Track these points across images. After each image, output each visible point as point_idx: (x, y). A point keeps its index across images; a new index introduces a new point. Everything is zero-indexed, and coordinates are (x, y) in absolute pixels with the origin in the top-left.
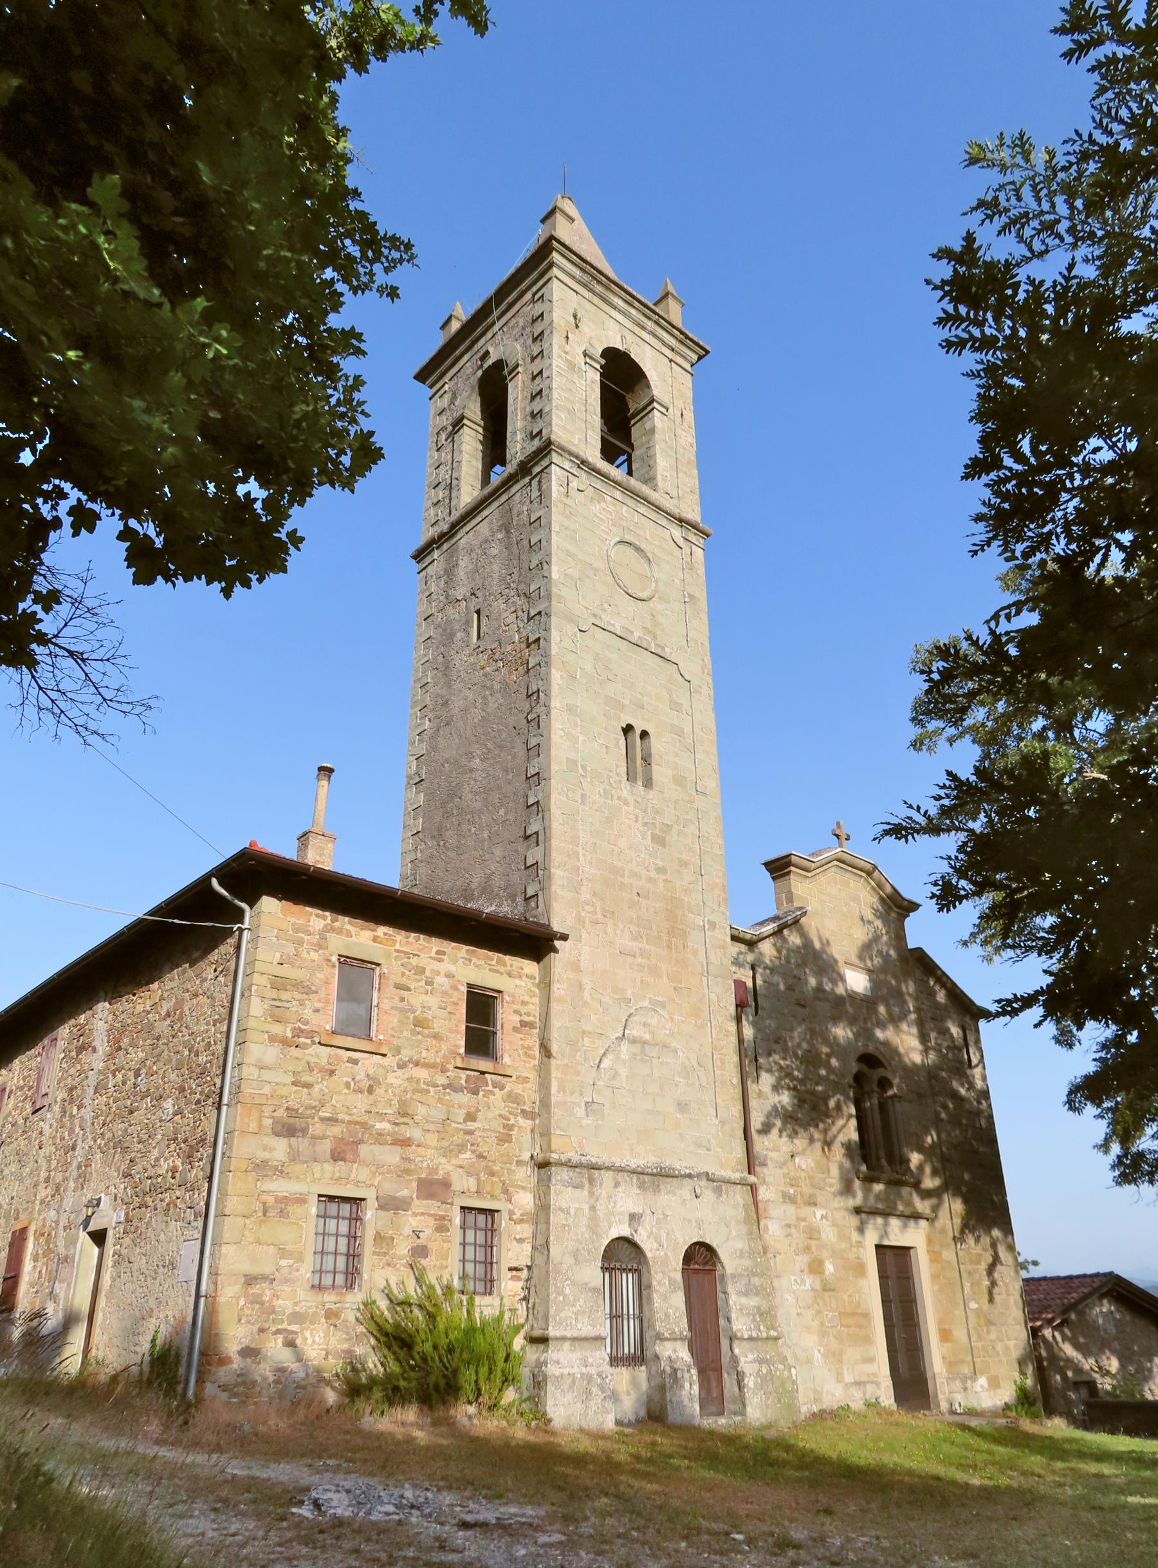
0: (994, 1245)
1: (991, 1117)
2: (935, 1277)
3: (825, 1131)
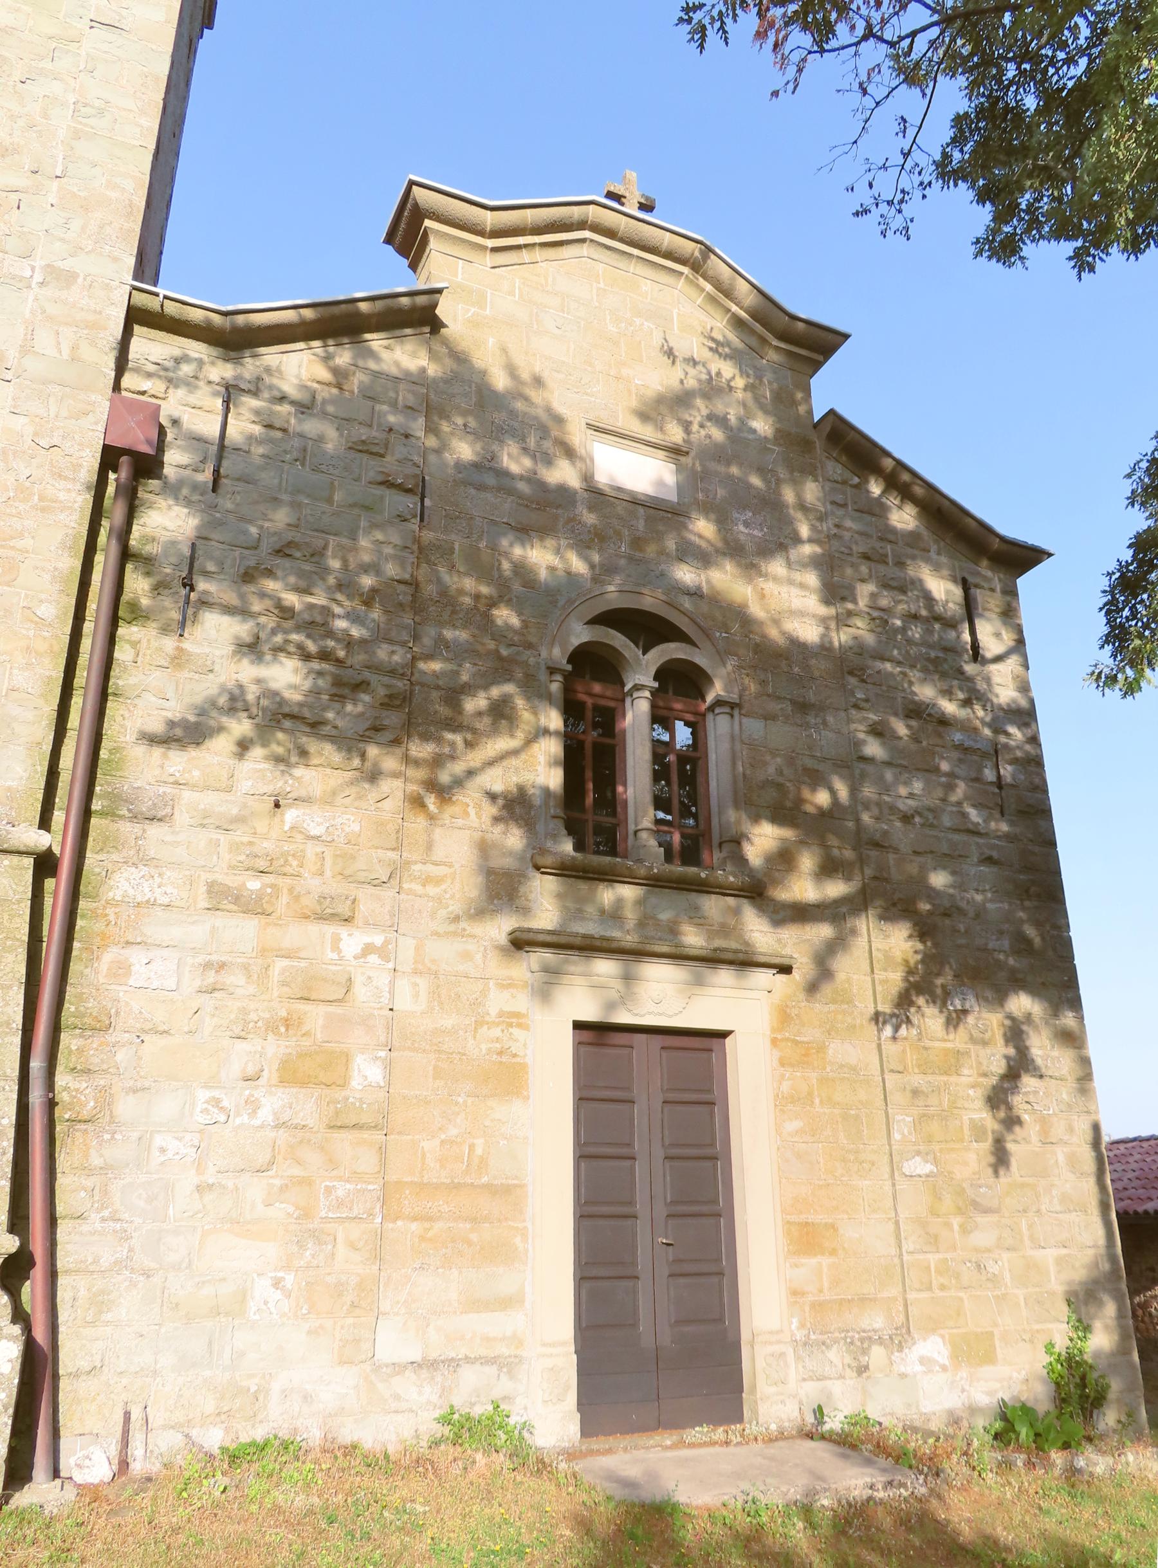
0: (1015, 1034)
1: (1036, 762)
2: (785, 1103)
3: (437, 762)
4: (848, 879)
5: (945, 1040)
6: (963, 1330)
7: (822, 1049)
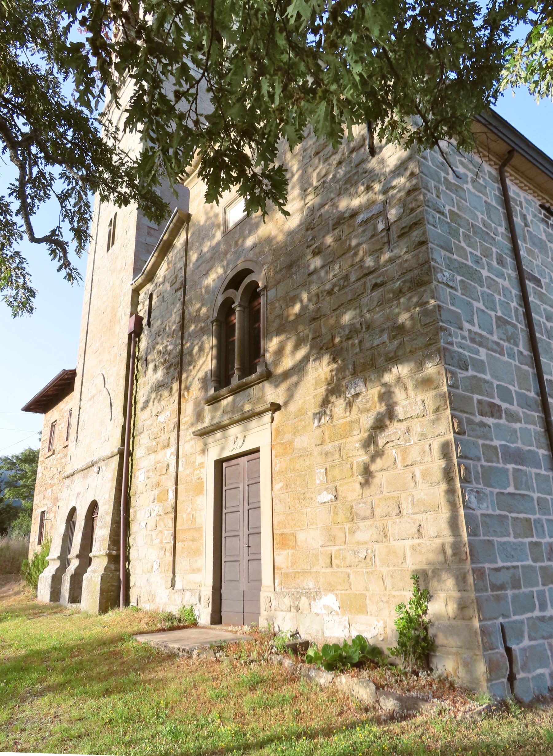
5: (345, 418)
6: (348, 592)
7: (291, 443)
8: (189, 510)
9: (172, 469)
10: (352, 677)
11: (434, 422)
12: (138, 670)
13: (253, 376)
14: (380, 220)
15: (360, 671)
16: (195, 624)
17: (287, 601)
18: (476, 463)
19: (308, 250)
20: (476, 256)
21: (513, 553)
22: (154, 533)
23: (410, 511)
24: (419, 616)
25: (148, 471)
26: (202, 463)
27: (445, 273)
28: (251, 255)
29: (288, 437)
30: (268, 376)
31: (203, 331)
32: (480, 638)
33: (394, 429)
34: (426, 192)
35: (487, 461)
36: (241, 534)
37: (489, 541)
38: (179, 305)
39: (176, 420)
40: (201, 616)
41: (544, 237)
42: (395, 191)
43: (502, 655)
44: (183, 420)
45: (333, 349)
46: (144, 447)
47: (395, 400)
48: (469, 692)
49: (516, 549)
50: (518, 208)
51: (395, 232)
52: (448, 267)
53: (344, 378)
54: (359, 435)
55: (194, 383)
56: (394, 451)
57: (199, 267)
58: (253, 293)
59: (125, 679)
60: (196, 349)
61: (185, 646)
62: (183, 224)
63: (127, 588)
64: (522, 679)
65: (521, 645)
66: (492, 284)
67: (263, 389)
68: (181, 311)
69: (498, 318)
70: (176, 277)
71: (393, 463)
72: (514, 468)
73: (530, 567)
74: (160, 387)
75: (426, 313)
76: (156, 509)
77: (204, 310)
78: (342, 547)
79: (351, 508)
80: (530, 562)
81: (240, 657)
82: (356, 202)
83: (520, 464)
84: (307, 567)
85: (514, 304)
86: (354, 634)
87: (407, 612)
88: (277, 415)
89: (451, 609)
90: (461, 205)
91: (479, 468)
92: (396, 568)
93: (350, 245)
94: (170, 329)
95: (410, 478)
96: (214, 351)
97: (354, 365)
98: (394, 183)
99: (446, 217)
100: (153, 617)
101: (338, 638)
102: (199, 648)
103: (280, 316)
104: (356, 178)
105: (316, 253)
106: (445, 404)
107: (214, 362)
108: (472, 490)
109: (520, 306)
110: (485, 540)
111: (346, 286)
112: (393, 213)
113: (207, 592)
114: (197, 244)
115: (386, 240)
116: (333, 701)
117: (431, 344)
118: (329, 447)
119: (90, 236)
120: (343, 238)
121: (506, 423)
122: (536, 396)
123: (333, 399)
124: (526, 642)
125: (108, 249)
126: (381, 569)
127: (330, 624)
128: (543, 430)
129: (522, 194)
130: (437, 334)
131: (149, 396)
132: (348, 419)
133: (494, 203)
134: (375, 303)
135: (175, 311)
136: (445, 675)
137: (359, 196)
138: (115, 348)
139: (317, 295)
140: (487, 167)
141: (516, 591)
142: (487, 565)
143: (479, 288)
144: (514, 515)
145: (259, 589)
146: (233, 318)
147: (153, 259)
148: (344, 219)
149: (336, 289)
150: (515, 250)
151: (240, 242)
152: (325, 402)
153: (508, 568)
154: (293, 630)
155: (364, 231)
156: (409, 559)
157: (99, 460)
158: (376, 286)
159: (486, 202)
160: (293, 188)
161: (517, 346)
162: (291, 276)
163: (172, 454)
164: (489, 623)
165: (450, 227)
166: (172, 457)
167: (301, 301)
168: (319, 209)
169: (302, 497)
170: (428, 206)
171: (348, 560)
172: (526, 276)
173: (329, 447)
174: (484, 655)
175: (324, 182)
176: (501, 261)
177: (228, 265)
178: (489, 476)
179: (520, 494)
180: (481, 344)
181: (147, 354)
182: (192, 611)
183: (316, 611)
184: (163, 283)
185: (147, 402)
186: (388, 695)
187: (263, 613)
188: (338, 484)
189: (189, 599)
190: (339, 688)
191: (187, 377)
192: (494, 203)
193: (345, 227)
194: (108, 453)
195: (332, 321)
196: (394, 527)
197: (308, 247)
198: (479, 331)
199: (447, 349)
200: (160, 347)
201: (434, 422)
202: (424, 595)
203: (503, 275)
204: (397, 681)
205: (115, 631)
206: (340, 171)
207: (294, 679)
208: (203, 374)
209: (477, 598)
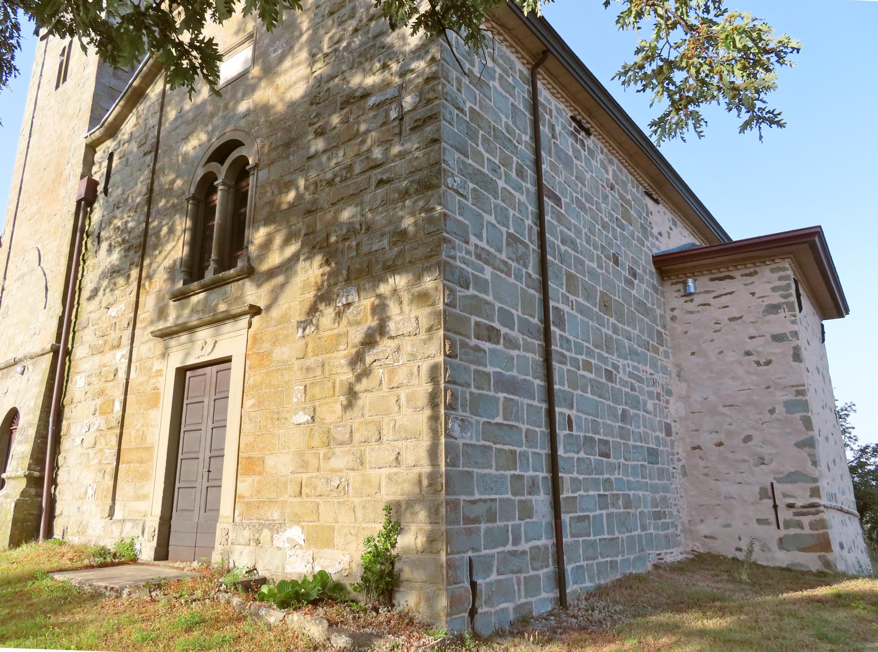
4: (296, 242)
5: (332, 329)
6: (316, 524)
7: (269, 354)
8: (139, 426)
9: (122, 375)
10: (305, 614)
11: (425, 342)
12: (48, 613)
13: (232, 271)
14: (393, 106)
15: (316, 608)
16: (134, 560)
17: (247, 533)
18: (464, 389)
19: (310, 129)
20: (494, 163)
21: (492, 486)
22: (92, 452)
23: (391, 438)
24: (387, 550)
25: (90, 376)
26: (160, 370)
27: (456, 178)
28: (243, 123)
29: (266, 346)
30: (250, 272)
31: (176, 208)
32: (445, 573)
33: (385, 346)
34: (446, 83)
35: (477, 388)
36: (201, 456)
37: (468, 472)
38: (147, 173)
39: (132, 315)
40: (143, 551)
41: (570, 153)
42: (413, 76)
43: (466, 589)
44: (141, 315)
45: (328, 250)
46: (87, 346)
47: (389, 314)
48: (427, 627)
49: (496, 481)
50: (547, 117)
51: (408, 123)
52: (461, 172)
53: (336, 284)
54: (344, 352)
55: (158, 271)
56: (381, 371)
57: (177, 128)
58: (241, 171)
59: (29, 623)
60: (165, 230)
61: (115, 584)
62: (160, 71)
63: (51, 517)
64: (484, 613)
65: (488, 580)
66: (508, 197)
67: (242, 288)
68: (149, 181)
69: (509, 235)
70: (146, 137)
71: (378, 383)
72: (505, 397)
73: (509, 500)
74: (114, 272)
75: (430, 221)
76: (96, 423)
77: (179, 183)
78: (314, 475)
79: (329, 431)
80: (509, 496)
81: (181, 596)
82: (370, 80)
83: (512, 394)
84: (273, 496)
85: (529, 222)
86: (317, 569)
87: (375, 546)
88: (256, 320)
89: (421, 541)
90: (484, 103)
91: (468, 396)
92: (369, 498)
93: (358, 130)
94: (133, 201)
95: (394, 401)
96: (188, 236)
97: (348, 270)
98: (413, 66)
99: (466, 115)
100: (79, 552)
101: (299, 573)
102: (130, 586)
103: (271, 203)
104: (372, 51)
105: (320, 133)
106: (439, 323)
107: (186, 248)
108: (456, 418)
109: (535, 224)
110: (464, 471)
111: (349, 178)
112: (408, 101)
113: (153, 523)
114: (177, 99)
115: (397, 130)
116: (280, 640)
117: (432, 256)
118: (311, 361)
119: (15, 69)
120: (351, 120)
121: (504, 349)
122: (539, 323)
123: (322, 307)
124: (494, 577)
125: (57, 87)
126: (353, 499)
127: (291, 559)
128: (541, 359)
129: (554, 101)
130: (439, 246)
131: (99, 283)
132: (335, 331)
133: (521, 107)
134: (378, 202)
135: (142, 179)
136: (406, 611)
137: (374, 74)
138: (58, 217)
139: (316, 184)
140: (519, 66)
141: (490, 525)
142: (463, 497)
143: (493, 199)
144: (498, 446)
145: (216, 520)
146: (215, 198)
147: (118, 109)
148: (354, 98)
149: (338, 179)
150: (538, 163)
151: (231, 105)
152: (313, 310)
153: (485, 501)
154: (251, 566)
155: (375, 117)
156: (384, 490)
157: (25, 358)
158: (381, 183)
159: (512, 104)
160: (301, 49)
161: (527, 268)
162: (287, 157)
163: (123, 356)
164: (457, 556)
165: (468, 127)
166: (123, 360)
167: (297, 188)
168: (328, 81)
169: (276, 416)
170: (446, 100)
171: (319, 489)
172: (545, 192)
173: (311, 361)
174: (447, 590)
175: (336, 50)
176: (520, 173)
177: (213, 131)
178: (476, 404)
179: (508, 425)
180: (487, 262)
181: (101, 228)
182: (132, 545)
183: (278, 545)
184: (129, 141)
185: (95, 292)
186: (340, 632)
187: (218, 548)
188: (317, 404)
189: (130, 531)
190: (290, 626)
191: (151, 264)
192: (521, 107)
193: (354, 107)
194: (37, 349)
195: (329, 216)
196: (372, 454)
197: (311, 125)
198: (487, 247)
199: (448, 262)
200: (118, 223)
201: (425, 342)
202: (394, 528)
203: (521, 188)
204: (354, 618)
205: (28, 567)
206: (355, 39)
207: (240, 619)
208: (171, 261)
209: (447, 531)
